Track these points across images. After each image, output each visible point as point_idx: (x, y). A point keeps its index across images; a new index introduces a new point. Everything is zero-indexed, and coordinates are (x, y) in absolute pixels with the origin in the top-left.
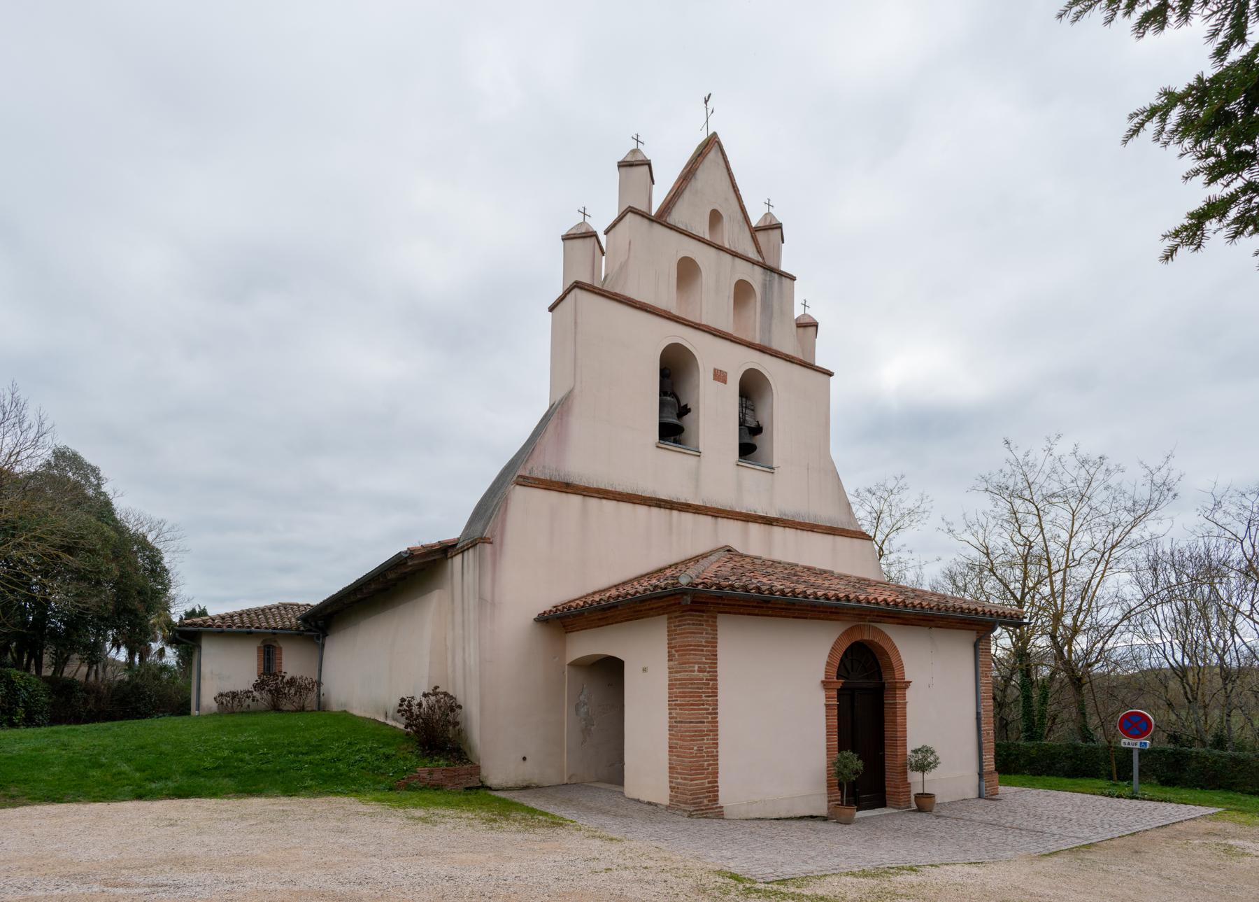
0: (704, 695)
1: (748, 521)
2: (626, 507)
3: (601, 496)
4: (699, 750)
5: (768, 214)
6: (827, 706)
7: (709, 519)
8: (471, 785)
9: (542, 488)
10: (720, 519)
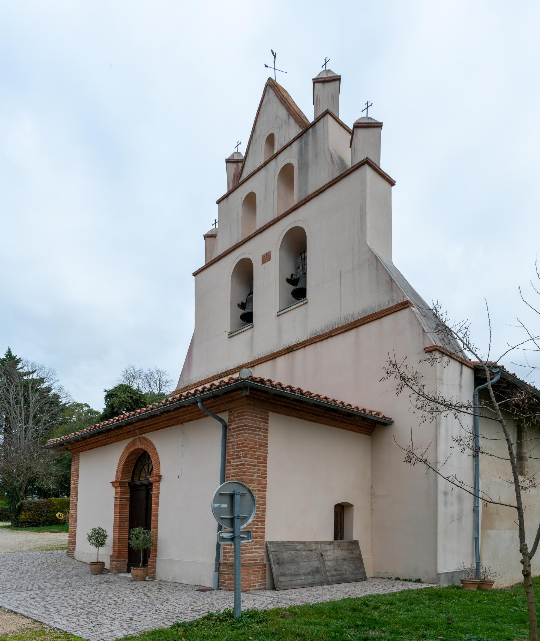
1: (275, 358)
6: (116, 498)
9: (270, 360)
10: (256, 367)
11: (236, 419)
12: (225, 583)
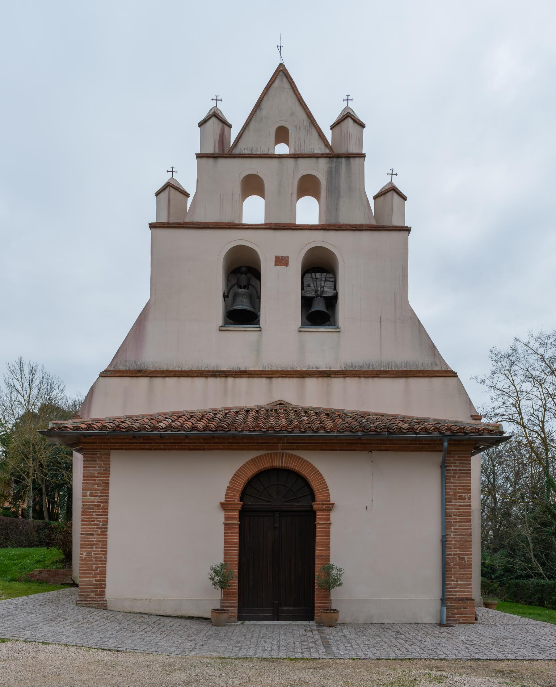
0: (94, 514)
1: (304, 377)
2: (185, 382)
3: (164, 375)
4: (88, 555)
5: (347, 107)
6: (226, 525)
7: (264, 381)
8: (66, 582)
9: (296, 377)
10: (274, 379)
11: (457, 462)
12: (455, 618)
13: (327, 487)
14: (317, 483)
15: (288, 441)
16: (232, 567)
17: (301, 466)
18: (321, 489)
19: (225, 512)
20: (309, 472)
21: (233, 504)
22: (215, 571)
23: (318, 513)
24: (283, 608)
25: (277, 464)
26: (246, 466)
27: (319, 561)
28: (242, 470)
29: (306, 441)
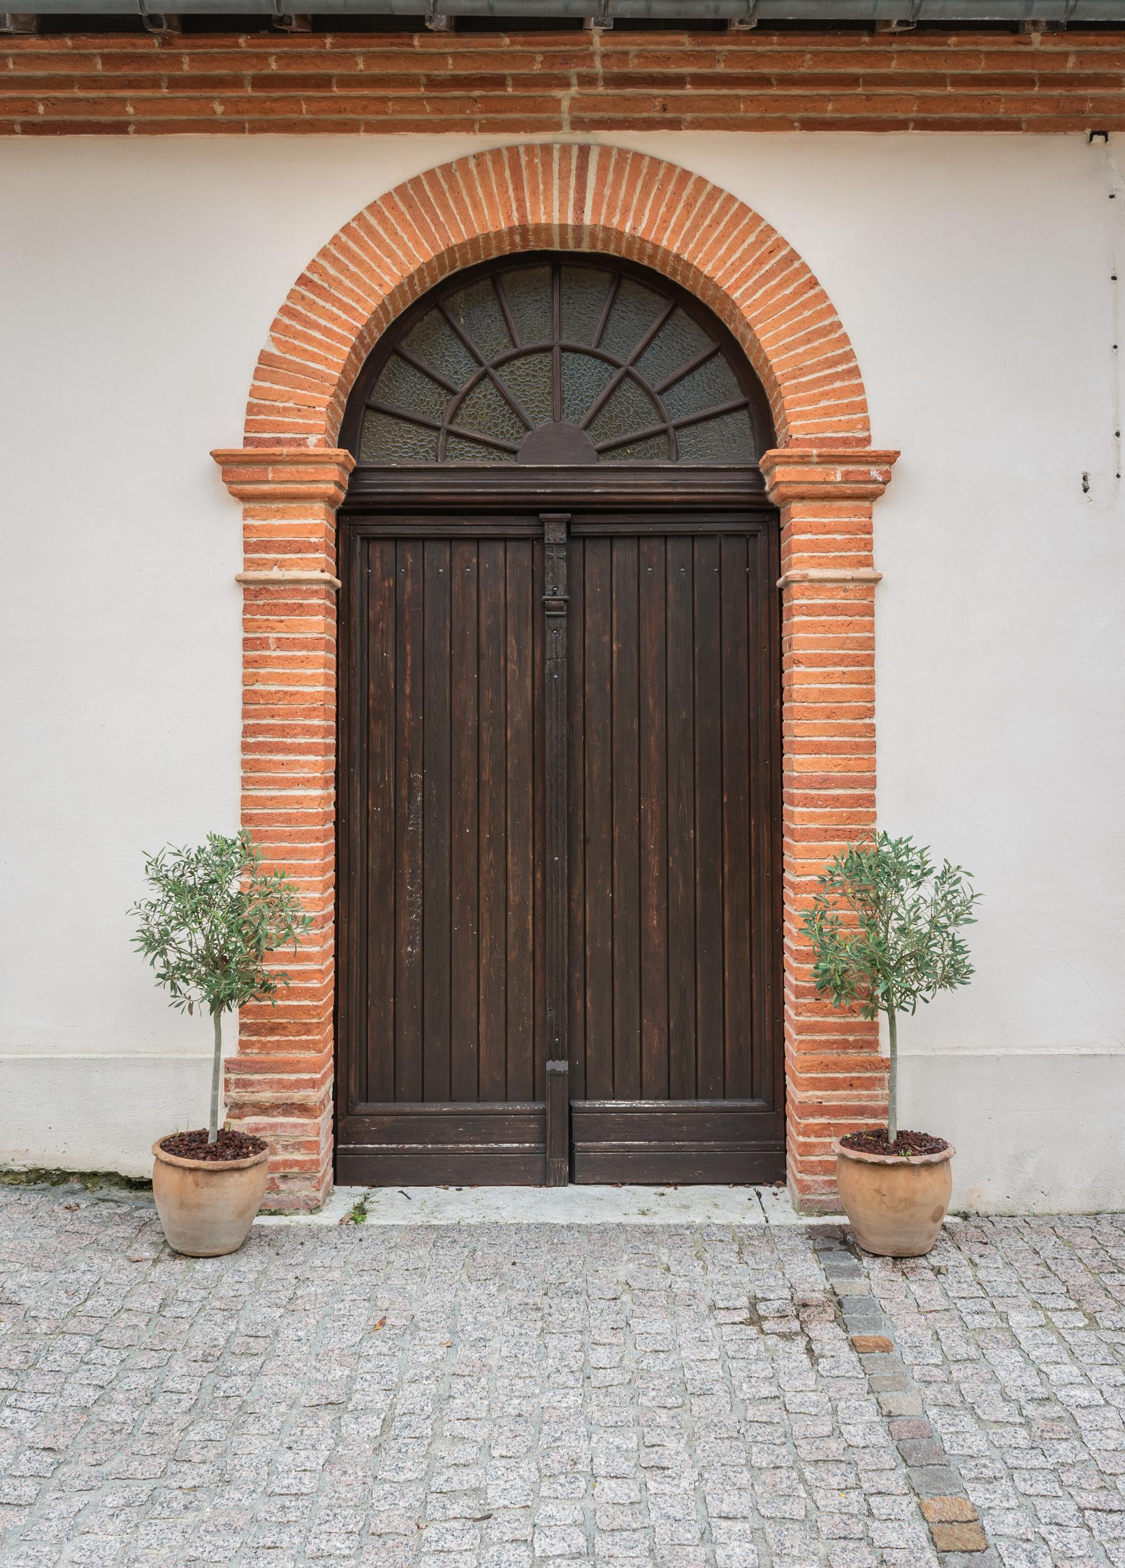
13: (850, 356)
14: (793, 330)
15: (615, 70)
16: (292, 853)
17: (695, 227)
18: (812, 369)
19: (247, 514)
20: (742, 260)
21: (294, 460)
22: (177, 889)
23: (798, 516)
24: (598, 1104)
25: (549, 213)
26: (371, 231)
27: (813, 818)
28: (345, 250)
29: (721, 69)
